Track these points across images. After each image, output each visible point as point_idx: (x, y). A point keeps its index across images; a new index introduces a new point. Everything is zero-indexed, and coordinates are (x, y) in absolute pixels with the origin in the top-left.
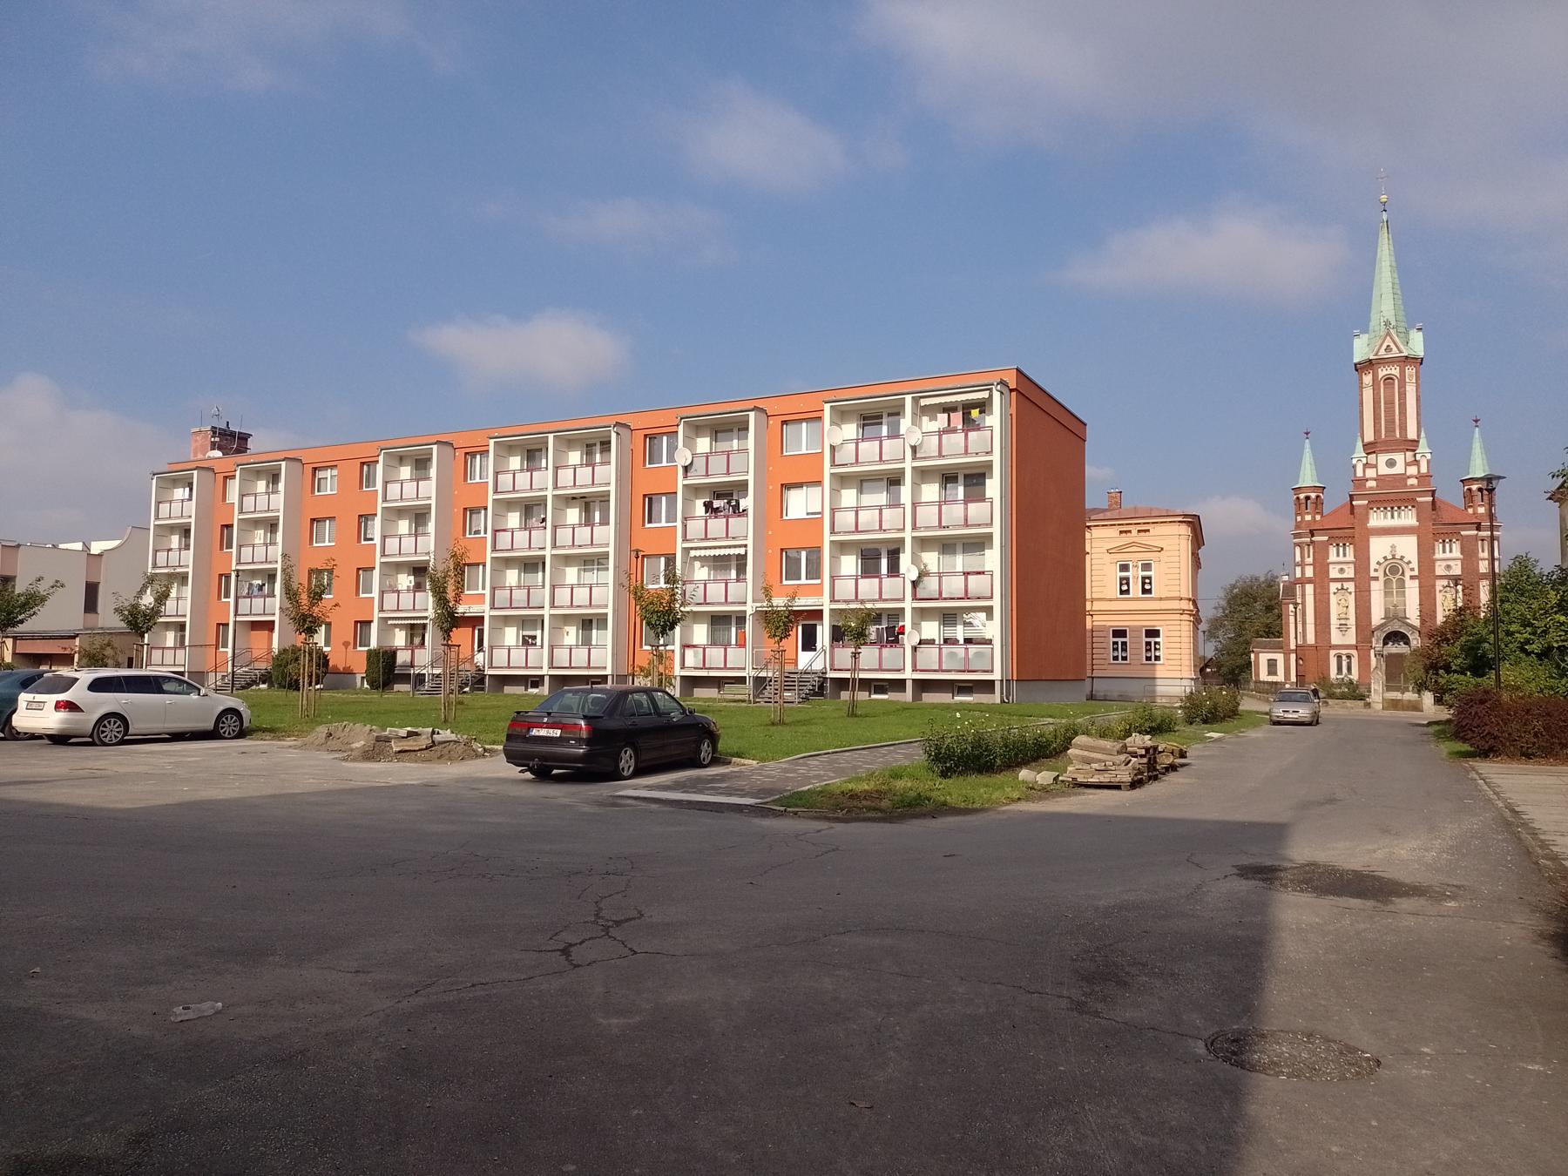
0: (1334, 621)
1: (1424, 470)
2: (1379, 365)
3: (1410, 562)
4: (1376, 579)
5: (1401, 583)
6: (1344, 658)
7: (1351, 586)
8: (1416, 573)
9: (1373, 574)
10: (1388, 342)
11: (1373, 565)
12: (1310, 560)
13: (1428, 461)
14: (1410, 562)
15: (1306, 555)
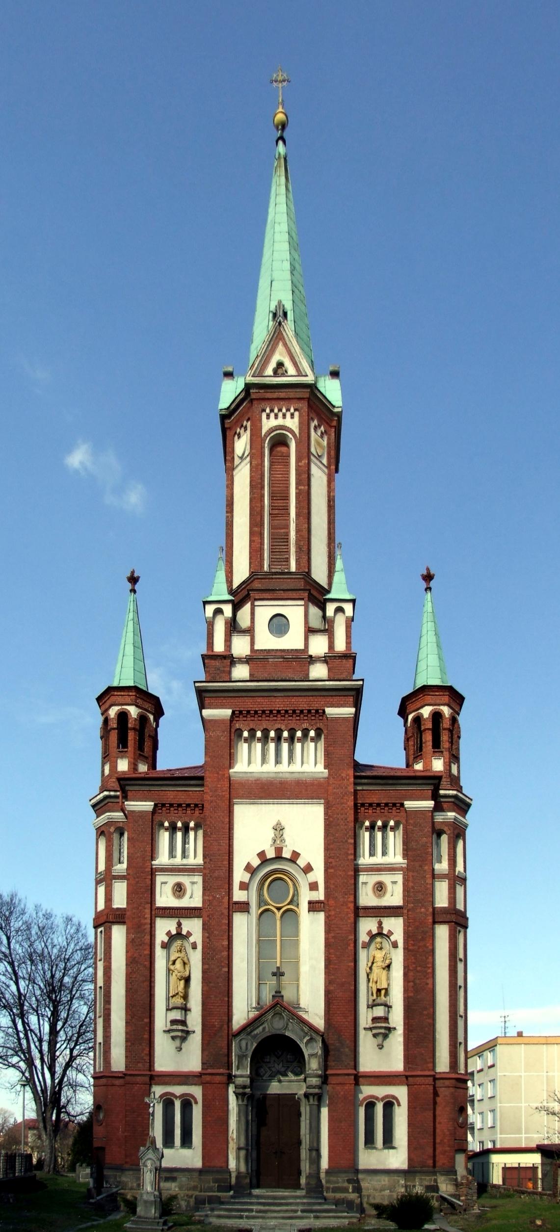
0: (161, 1018)
1: (340, 645)
2: (263, 405)
3: (308, 869)
4: (244, 907)
5: (290, 915)
6: (178, 1104)
7: (194, 927)
8: (320, 895)
9: (239, 895)
10: (280, 355)
11: (239, 875)
12: (121, 868)
13: (350, 621)
14: (308, 869)
15: (115, 859)
